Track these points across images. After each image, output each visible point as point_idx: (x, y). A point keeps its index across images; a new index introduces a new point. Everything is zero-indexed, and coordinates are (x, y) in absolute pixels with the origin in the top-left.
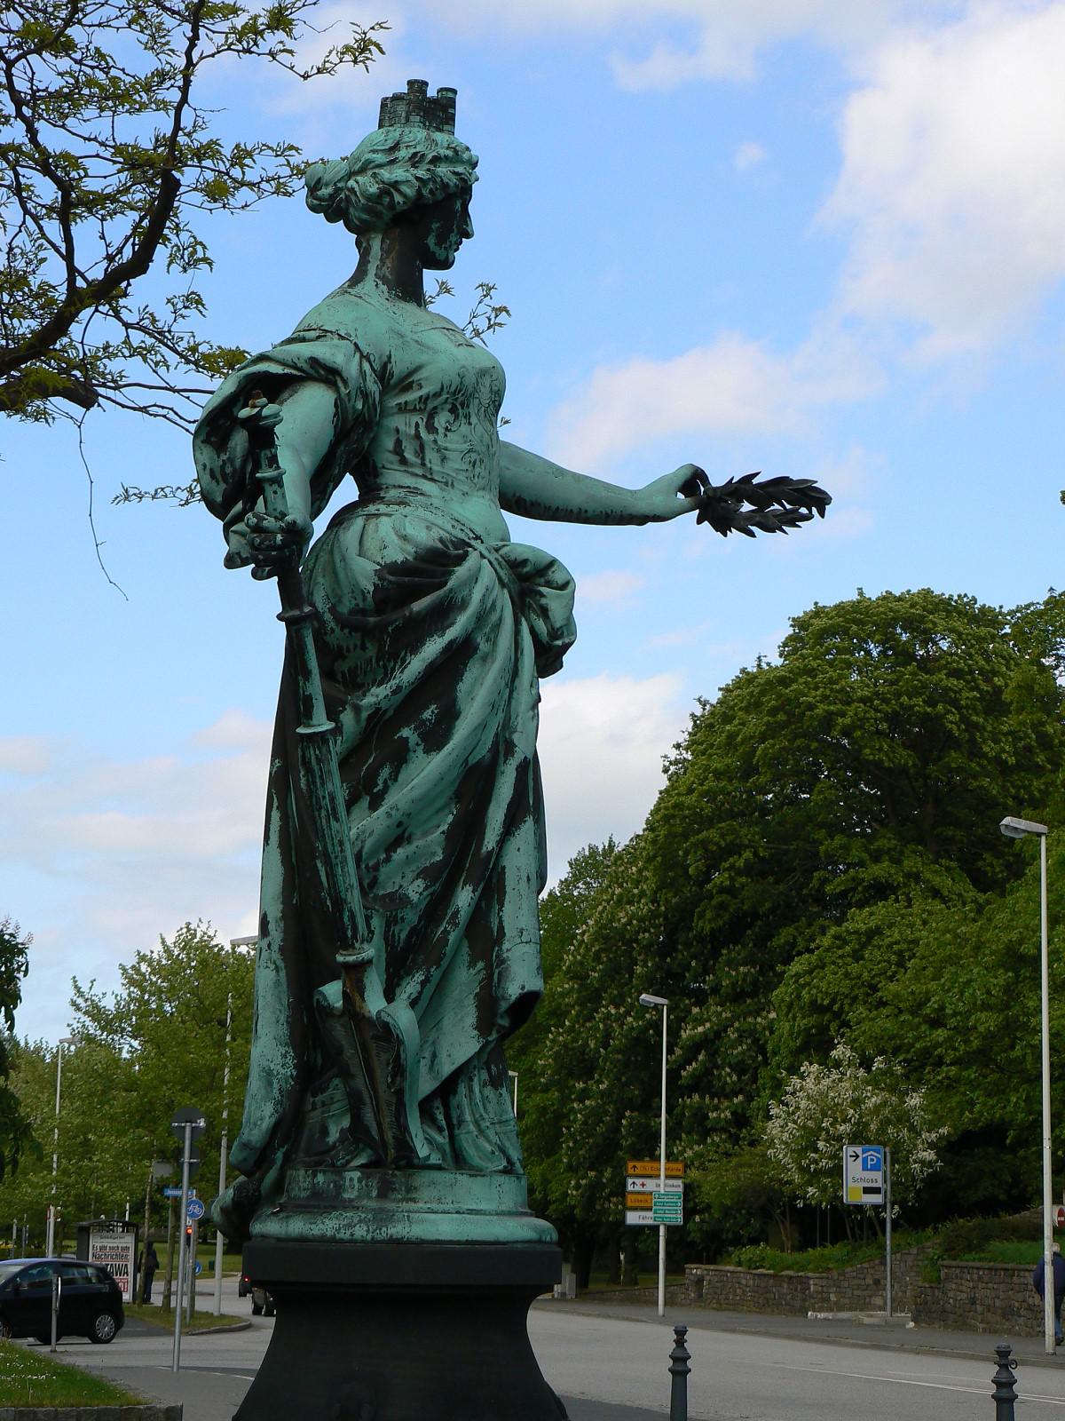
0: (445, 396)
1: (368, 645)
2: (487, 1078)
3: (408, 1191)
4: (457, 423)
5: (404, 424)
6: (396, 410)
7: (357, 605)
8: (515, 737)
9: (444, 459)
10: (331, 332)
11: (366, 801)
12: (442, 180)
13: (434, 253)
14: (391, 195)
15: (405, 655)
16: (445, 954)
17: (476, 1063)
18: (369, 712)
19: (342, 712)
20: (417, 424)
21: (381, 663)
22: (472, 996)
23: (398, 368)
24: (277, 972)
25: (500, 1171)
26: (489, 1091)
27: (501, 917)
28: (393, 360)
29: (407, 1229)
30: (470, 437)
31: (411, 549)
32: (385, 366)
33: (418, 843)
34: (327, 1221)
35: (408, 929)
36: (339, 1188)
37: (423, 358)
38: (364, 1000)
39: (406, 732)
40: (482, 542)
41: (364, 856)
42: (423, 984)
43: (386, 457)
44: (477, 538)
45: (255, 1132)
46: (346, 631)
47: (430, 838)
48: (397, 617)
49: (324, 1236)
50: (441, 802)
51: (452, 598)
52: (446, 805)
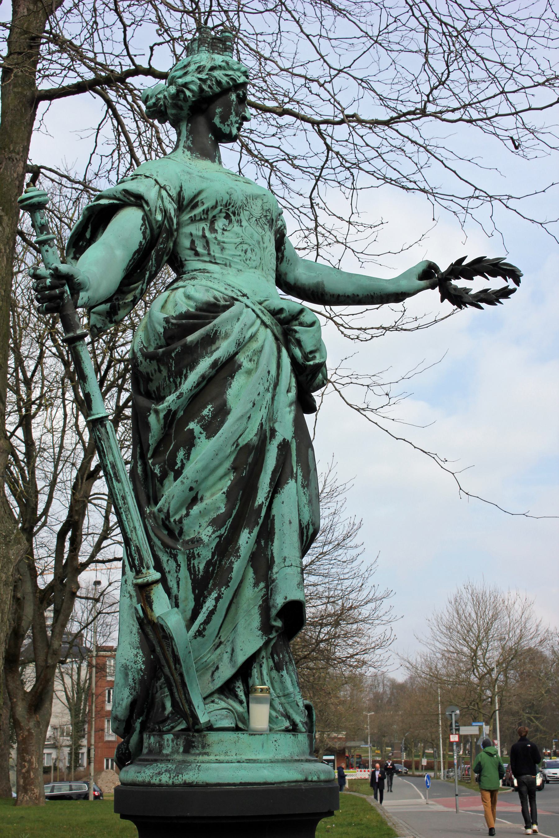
0: (219, 208)
1: (162, 368)
2: (273, 665)
3: (203, 747)
4: (231, 226)
5: (196, 229)
6: (189, 221)
7: (157, 344)
8: (277, 426)
9: (223, 249)
10: (141, 175)
11: (172, 475)
12: (216, 79)
13: (220, 129)
14: (183, 92)
15: (187, 372)
16: (231, 578)
17: (263, 653)
18: (165, 413)
19: (149, 415)
20: (203, 229)
21: (171, 380)
22: (257, 607)
23: (188, 194)
24: (131, 599)
25: (283, 731)
26: (274, 673)
27: (272, 550)
28: (183, 189)
29: (196, 776)
30: (242, 234)
31: (192, 304)
32: (179, 194)
33: (208, 501)
34: (147, 771)
35: (205, 562)
36: (161, 747)
37: (203, 186)
38: (152, 610)
39: (192, 425)
40: (248, 298)
41: (171, 513)
42: (217, 600)
43: (186, 254)
44: (244, 295)
45: (119, 709)
46: (148, 360)
47: (214, 498)
48: (177, 347)
49: (144, 782)
50: (221, 471)
51: (216, 331)
52: (225, 475)
